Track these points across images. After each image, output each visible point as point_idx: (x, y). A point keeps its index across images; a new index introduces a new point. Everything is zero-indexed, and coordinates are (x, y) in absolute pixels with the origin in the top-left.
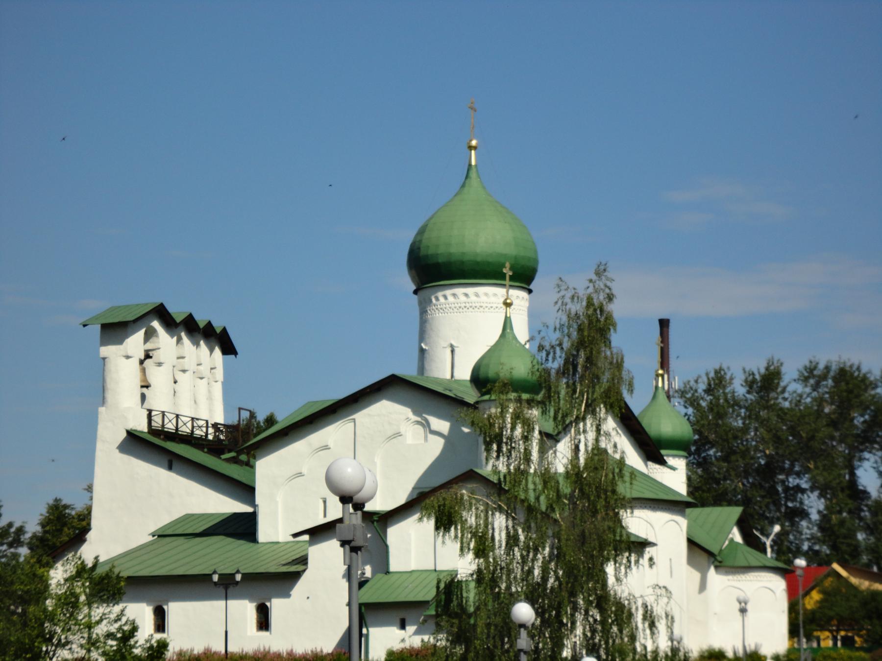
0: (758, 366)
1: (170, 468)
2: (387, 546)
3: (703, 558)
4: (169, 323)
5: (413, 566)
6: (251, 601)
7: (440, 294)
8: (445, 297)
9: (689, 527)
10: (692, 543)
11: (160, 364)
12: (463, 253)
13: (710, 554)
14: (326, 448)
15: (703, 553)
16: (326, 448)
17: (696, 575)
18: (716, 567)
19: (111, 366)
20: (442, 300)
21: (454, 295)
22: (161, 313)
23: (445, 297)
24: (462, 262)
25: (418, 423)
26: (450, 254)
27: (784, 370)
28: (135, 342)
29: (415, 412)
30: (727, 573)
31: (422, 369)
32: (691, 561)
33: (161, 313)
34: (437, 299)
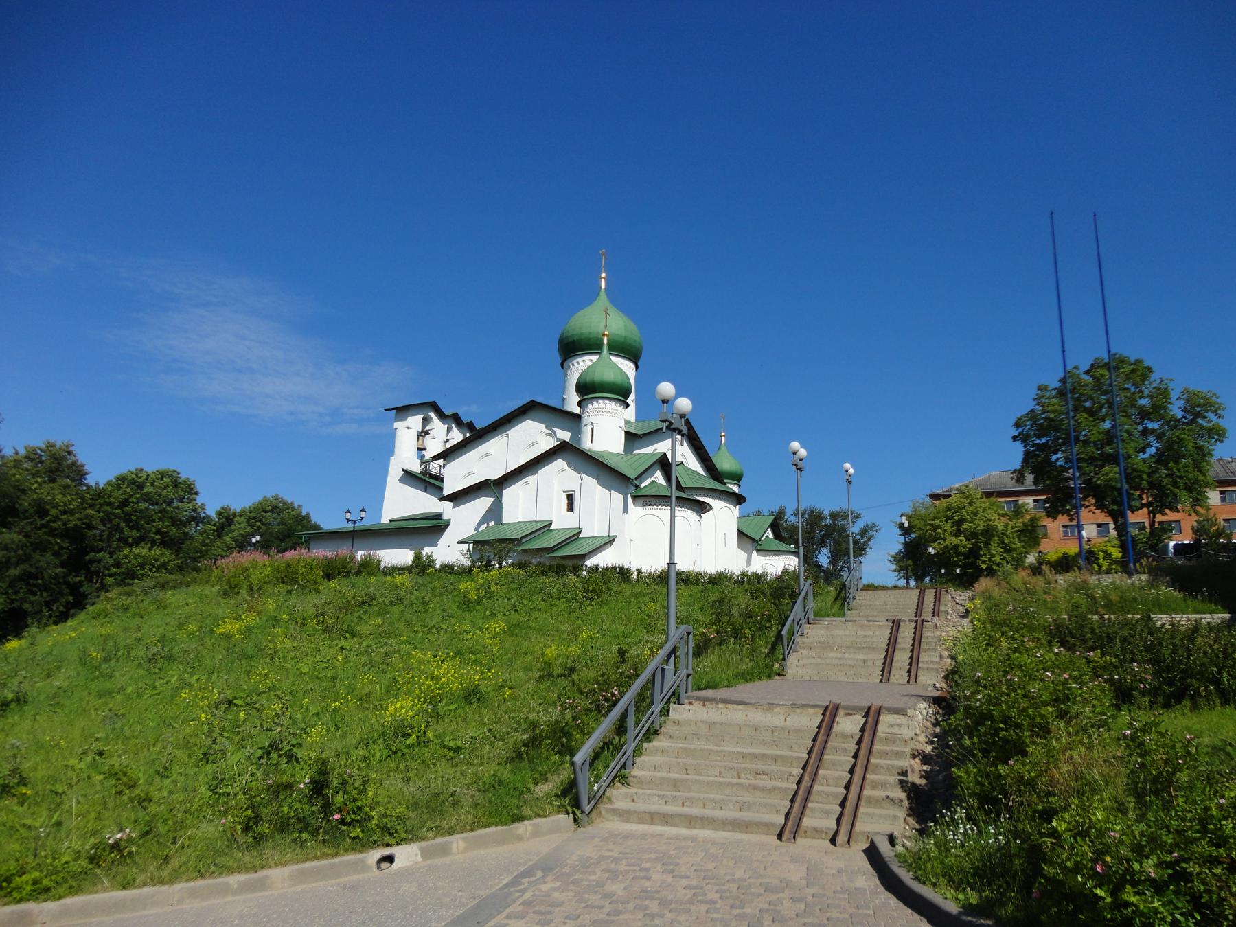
0: (775, 509)
1: (425, 491)
2: (501, 503)
3: (749, 544)
4: (442, 416)
5: (520, 518)
6: (411, 550)
7: (575, 361)
8: (578, 363)
9: (741, 518)
10: (741, 533)
11: (434, 438)
12: (590, 333)
13: (753, 540)
14: (489, 454)
15: (748, 540)
16: (489, 454)
17: (745, 555)
18: (757, 551)
19: (399, 433)
20: (576, 365)
21: (584, 361)
22: (434, 407)
23: (578, 363)
24: (590, 339)
25: (549, 434)
26: (581, 334)
27: (786, 511)
28: (415, 421)
29: (547, 428)
30: (765, 555)
31: (563, 406)
32: (740, 545)
33: (434, 407)
34: (573, 365)
